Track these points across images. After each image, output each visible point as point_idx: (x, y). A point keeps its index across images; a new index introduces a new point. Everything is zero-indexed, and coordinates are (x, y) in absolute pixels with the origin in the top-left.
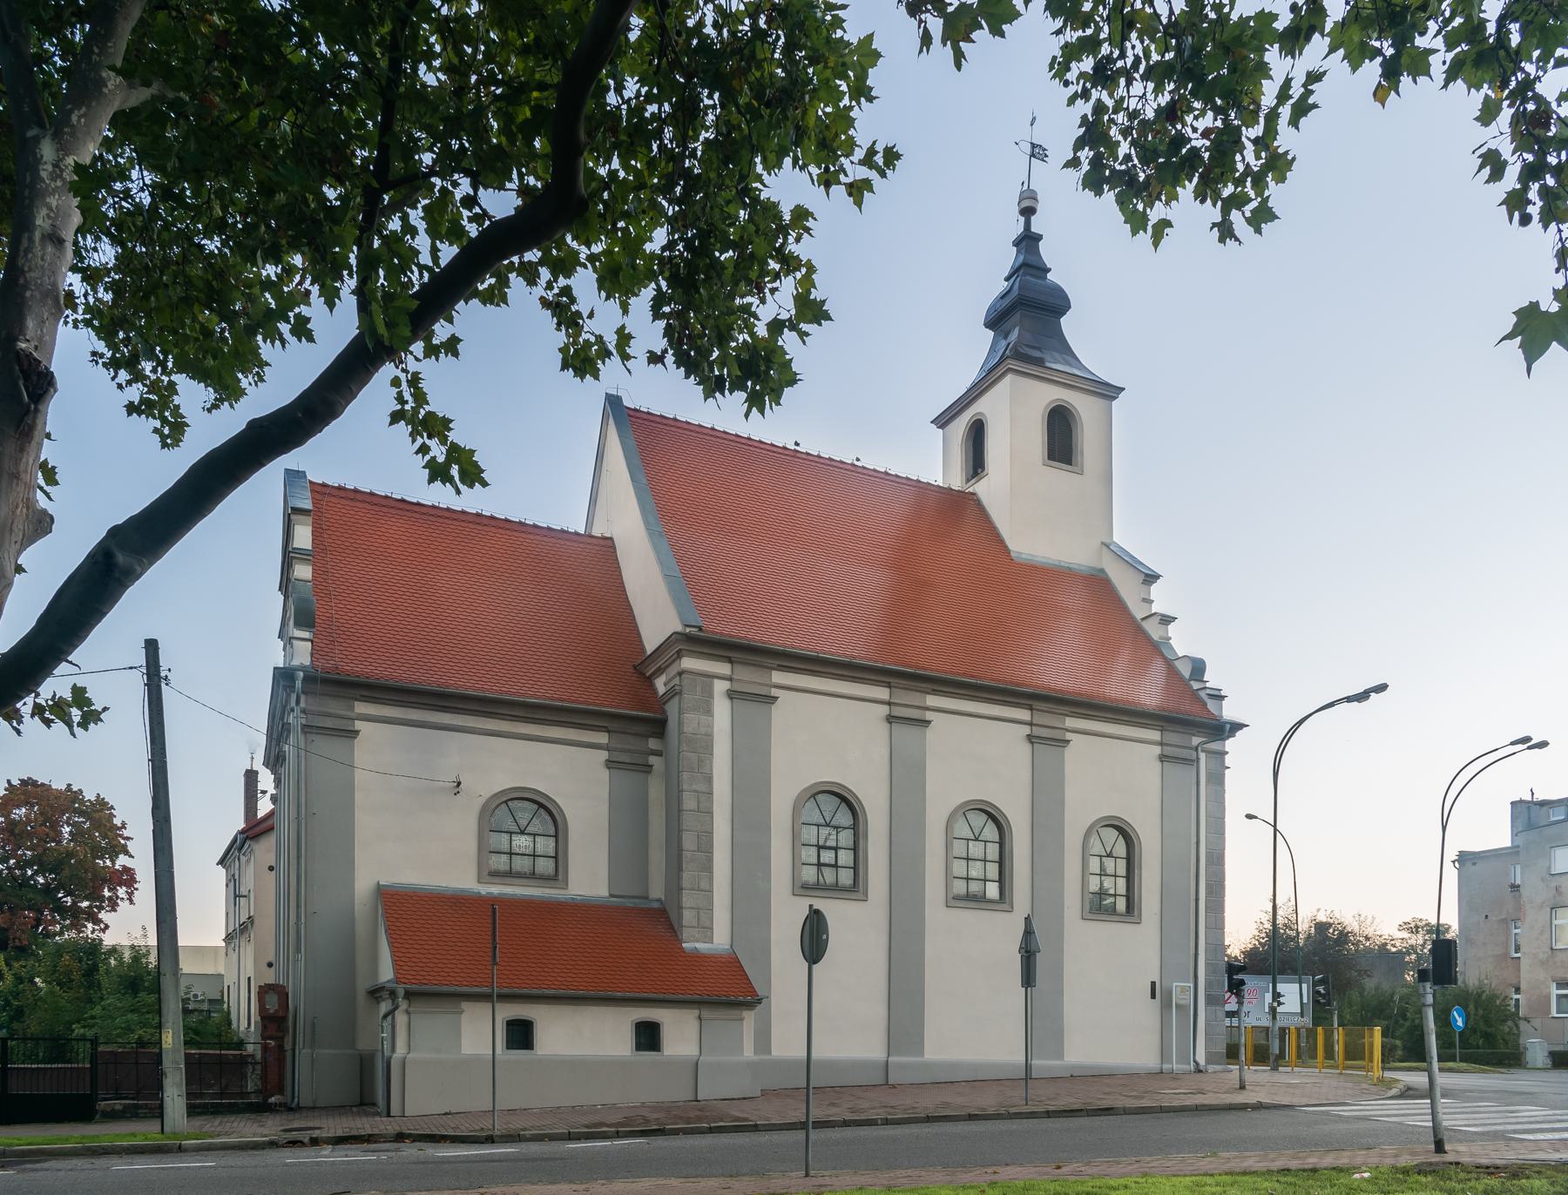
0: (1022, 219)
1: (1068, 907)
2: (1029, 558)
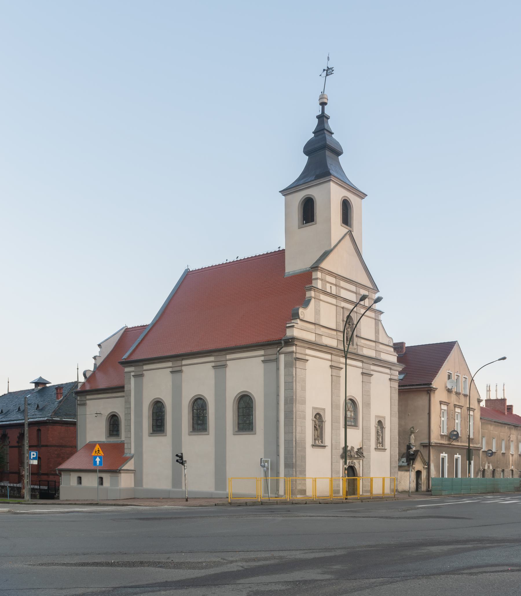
0: (321, 107)
1: (467, 442)
2: (293, 272)
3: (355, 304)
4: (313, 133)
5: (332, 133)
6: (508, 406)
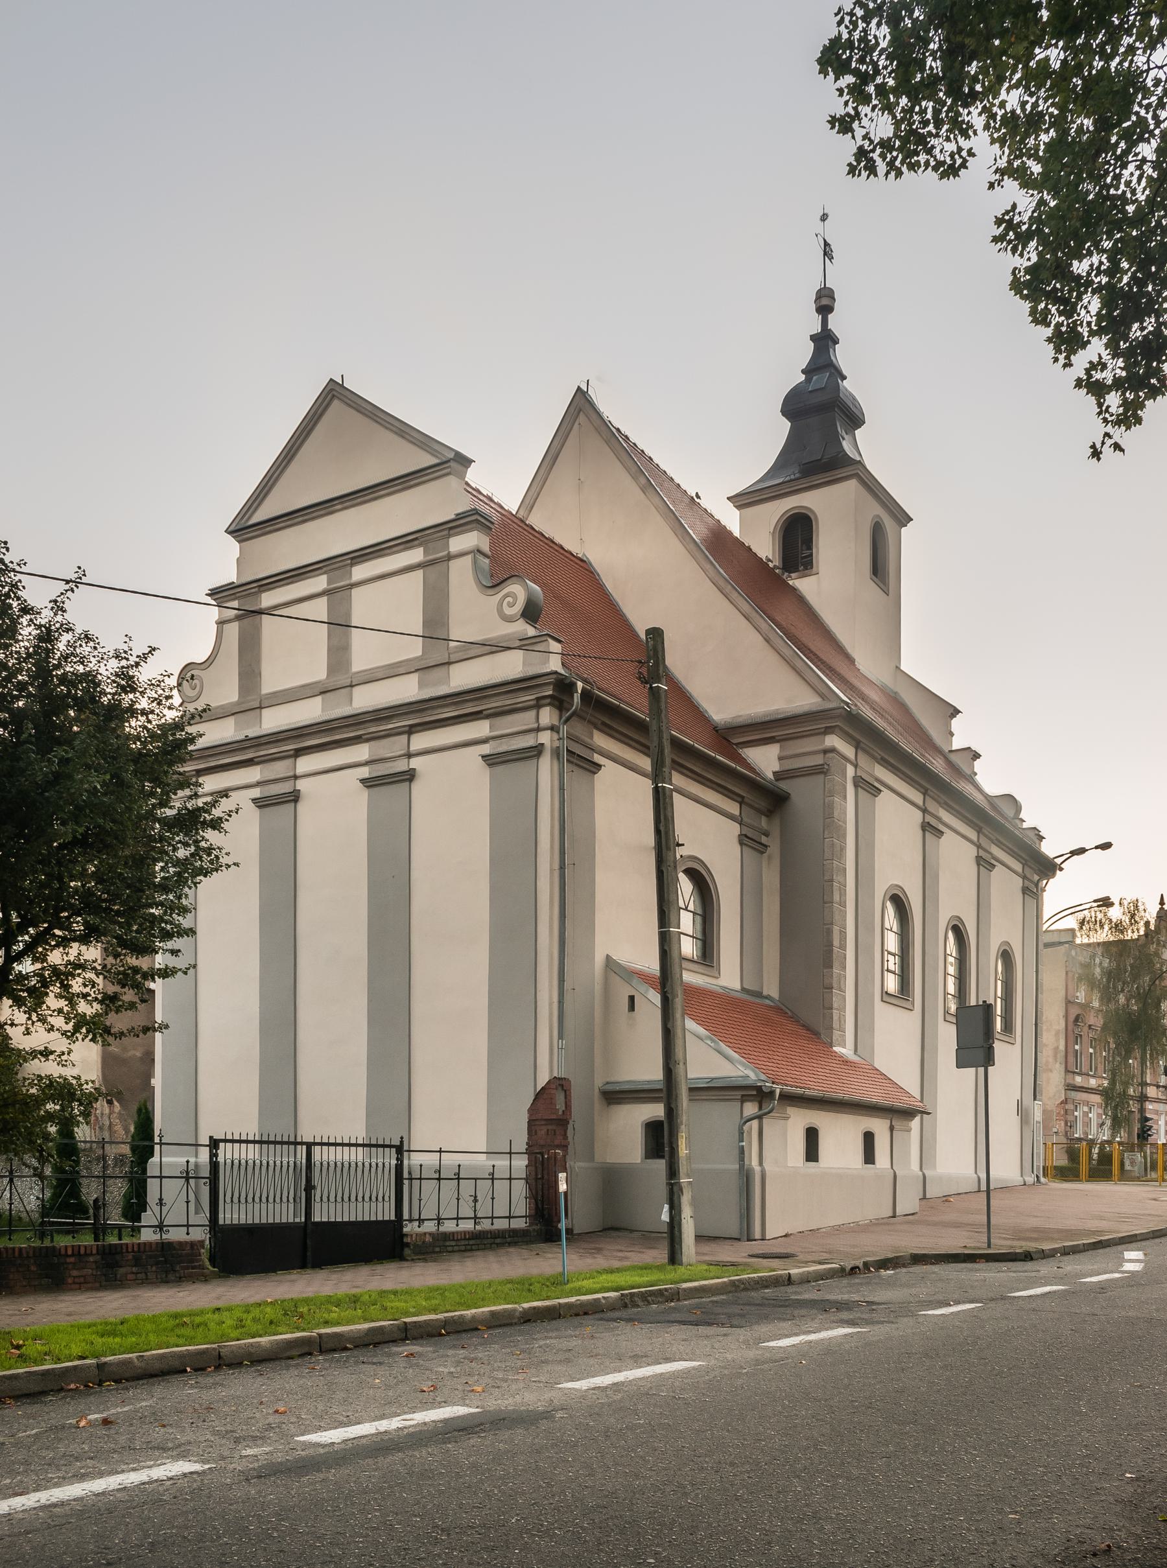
3: (372, 677)
4: (803, 372)
5: (844, 378)
6: (662, 1157)
